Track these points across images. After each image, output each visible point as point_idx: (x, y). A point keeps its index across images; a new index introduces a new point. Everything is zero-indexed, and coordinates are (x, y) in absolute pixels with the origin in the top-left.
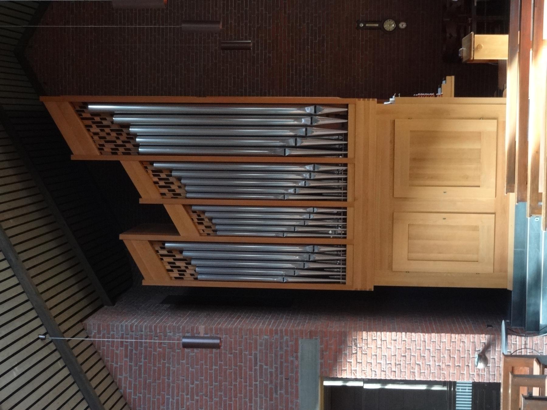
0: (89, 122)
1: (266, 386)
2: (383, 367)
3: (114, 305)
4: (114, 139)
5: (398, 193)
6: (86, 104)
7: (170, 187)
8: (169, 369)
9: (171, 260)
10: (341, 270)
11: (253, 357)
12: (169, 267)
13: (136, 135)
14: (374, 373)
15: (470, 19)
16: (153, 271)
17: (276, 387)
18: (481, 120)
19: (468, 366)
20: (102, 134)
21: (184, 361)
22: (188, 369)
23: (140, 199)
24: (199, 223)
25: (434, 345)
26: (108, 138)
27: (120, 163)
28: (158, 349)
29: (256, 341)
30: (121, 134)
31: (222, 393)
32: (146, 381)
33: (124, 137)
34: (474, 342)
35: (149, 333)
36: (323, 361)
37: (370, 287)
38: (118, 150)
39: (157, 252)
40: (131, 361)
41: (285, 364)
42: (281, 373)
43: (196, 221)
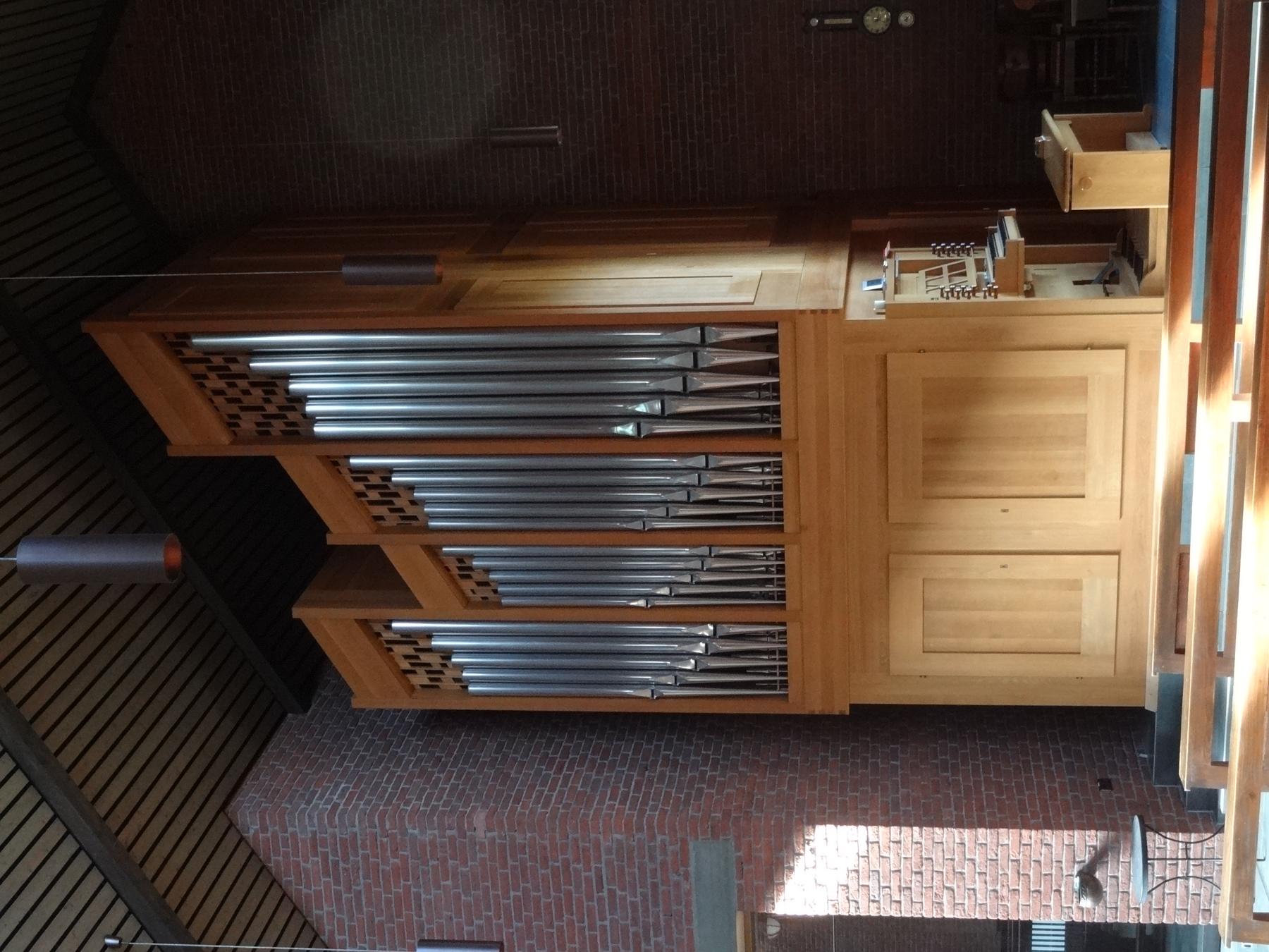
0: (200, 368)
1: (625, 930)
2: (874, 893)
3: (306, 710)
4: (260, 402)
5: (895, 516)
6: (187, 336)
7: (391, 503)
8: (418, 897)
9: (409, 650)
10: (777, 671)
11: (592, 874)
12: (405, 665)
13: (302, 399)
14: (853, 904)
15: (1059, 26)
16: (369, 683)
17: (646, 931)
18: (1089, 352)
19: (1058, 891)
20: (231, 393)
21: (449, 883)
22: (458, 897)
23: (328, 536)
24: (462, 576)
25: (983, 851)
26: (247, 401)
27: (277, 462)
28: (392, 861)
29: (597, 846)
30: (274, 393)
31: (534, 942)
32: (373, 922)
33: (282, 408)
34: (1071, 846)
35: (368, 830)
36: (742, 882)
37: (841, 707)
38: (269, 425)
39: (379, 635)
40: (337, 882)
41: (661, 888)
42: (656, 904)
43: (455, 572)
